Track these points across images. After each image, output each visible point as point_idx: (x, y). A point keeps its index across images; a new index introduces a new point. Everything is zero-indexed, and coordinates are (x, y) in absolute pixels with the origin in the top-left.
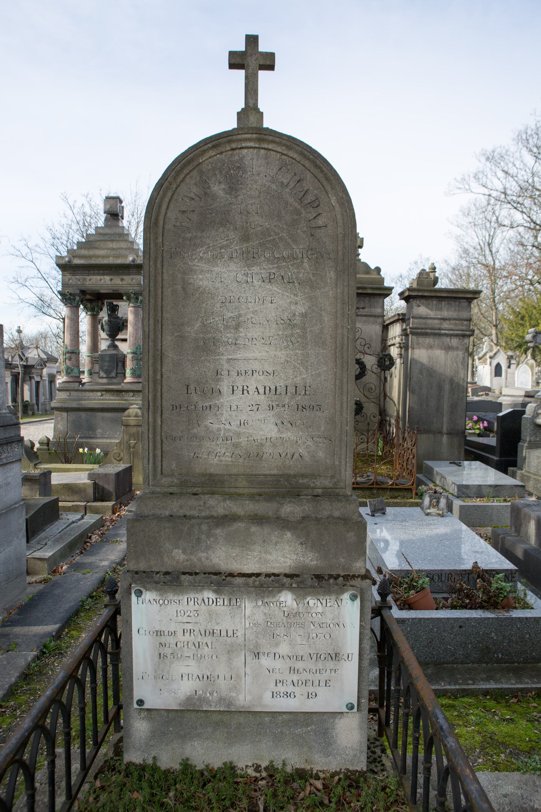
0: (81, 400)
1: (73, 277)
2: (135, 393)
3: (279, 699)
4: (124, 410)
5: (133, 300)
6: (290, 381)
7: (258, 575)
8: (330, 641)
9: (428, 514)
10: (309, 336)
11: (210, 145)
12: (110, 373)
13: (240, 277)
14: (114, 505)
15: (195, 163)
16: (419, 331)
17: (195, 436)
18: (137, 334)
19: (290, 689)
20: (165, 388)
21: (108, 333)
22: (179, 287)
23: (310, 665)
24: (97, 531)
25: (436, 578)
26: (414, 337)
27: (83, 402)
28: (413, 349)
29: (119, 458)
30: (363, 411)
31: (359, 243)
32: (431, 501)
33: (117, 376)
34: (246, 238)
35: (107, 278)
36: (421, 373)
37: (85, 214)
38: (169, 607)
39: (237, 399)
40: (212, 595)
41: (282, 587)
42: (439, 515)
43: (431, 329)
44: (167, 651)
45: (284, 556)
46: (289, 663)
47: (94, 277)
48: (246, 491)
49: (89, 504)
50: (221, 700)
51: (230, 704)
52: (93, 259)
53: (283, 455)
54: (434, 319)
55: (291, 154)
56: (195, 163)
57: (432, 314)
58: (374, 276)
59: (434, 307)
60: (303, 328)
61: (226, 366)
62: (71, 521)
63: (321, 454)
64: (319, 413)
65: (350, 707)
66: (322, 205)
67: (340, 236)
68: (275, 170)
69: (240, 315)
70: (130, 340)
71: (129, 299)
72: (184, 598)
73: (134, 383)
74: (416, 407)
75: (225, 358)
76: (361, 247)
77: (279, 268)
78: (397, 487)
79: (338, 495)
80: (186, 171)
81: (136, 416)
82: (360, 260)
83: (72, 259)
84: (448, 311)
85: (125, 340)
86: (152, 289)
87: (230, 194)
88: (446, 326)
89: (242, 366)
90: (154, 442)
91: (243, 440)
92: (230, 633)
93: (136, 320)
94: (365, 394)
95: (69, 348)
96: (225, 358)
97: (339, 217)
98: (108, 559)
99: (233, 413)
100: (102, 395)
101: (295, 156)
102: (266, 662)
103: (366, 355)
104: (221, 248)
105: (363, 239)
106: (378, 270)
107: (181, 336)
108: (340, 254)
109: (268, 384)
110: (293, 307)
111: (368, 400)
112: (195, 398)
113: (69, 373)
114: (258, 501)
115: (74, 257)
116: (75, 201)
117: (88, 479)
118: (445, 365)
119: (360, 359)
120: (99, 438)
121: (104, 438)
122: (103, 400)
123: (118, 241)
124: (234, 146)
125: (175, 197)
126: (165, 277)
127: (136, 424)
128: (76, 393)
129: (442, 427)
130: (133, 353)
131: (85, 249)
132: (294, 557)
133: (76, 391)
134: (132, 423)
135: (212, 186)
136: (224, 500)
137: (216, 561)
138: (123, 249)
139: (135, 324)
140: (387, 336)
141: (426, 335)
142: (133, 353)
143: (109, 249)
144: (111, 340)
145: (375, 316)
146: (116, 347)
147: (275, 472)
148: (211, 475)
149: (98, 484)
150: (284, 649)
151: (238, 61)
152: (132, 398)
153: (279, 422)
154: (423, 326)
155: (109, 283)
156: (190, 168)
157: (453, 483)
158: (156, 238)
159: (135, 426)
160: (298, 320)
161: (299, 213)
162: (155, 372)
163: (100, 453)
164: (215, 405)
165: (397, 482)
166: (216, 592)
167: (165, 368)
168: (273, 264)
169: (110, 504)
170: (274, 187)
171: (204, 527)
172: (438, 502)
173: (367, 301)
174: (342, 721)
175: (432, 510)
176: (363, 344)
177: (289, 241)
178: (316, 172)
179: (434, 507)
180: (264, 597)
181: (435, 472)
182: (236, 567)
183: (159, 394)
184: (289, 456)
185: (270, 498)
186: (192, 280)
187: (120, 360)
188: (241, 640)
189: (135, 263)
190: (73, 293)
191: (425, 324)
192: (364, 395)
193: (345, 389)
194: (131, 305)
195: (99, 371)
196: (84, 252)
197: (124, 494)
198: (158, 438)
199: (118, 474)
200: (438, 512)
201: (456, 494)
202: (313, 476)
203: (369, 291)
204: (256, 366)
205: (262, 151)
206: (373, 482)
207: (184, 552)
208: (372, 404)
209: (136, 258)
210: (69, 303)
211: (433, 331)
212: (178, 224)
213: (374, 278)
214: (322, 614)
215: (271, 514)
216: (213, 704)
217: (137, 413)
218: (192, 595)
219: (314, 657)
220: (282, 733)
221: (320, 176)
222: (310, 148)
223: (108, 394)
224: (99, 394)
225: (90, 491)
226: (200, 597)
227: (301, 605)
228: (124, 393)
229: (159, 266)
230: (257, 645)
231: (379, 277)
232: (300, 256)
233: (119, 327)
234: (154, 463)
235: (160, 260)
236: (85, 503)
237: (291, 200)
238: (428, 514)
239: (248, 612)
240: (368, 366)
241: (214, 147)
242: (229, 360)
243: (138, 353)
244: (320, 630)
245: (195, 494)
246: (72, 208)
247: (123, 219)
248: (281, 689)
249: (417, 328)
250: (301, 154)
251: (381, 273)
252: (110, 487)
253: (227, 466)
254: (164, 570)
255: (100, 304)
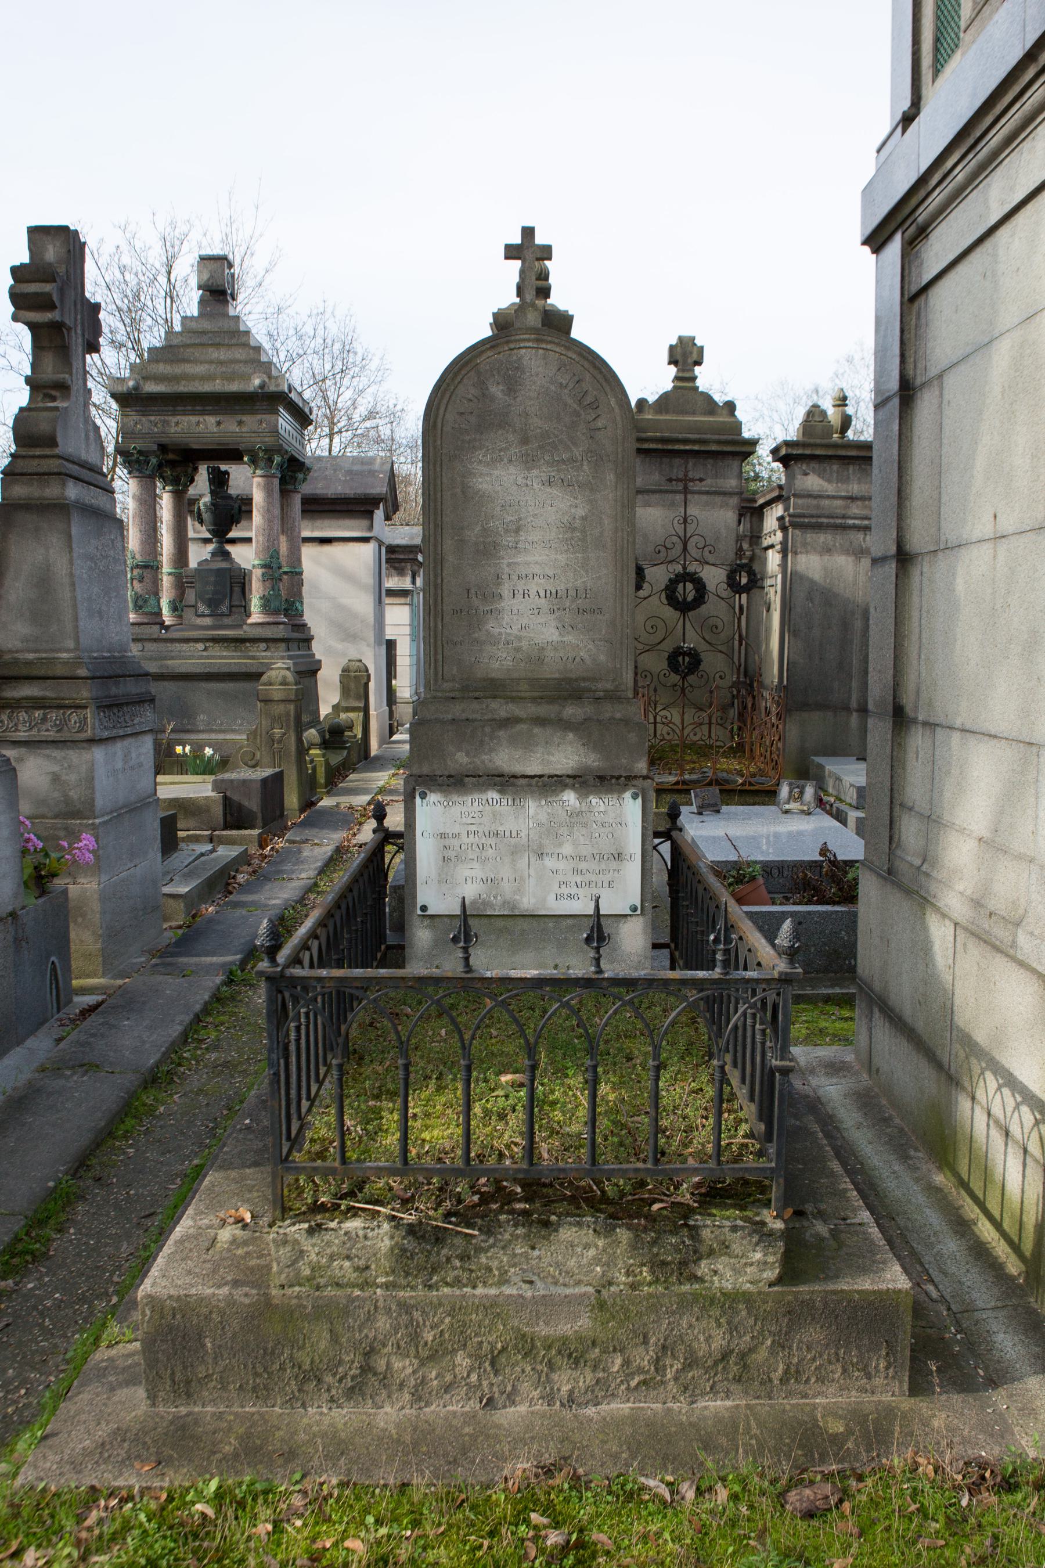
0: (165, 658)
1: (144, 419)
2: (270, 644)
3: (563, 902)
4: (256, 676)
5: (262, 464)
6: (570, 584)
7: (540, 776)
8: (612, 841)
9: (787, 812)
10: (589, 539)
11: (488, 346)
12: (217, 606)
13: (520, 481)
14: (260, 834)
15: (473, 364)
16: (806, 520)
17: (476, 640)
18: (271, 529)
19: (574, 890)
20: (445, 594)
21: (211, 528)
22: (458, 490)
23: (593, 865)
24: (245, 868)
25: (775, 872)
26: (797, 532)
27: (169, 662)
28: (796, 553)
29: (253, 762)
30: (701, 668)
31: (695, 357)
32: (791, 792)
33: (231, 611)
34: (525, 441)
35: (211, 420)
36: (810, 598)
37: (123, 270)
38: (453, 809)
39: (518, 603)
40: (496, 796)
41: (565, 786)
42: (803, 812)
43: (828, 517)
44: (452, 854)
45: (566, 757)
46: (572, 864)
47: (186, 418)
48: (528, 694)
49: (217, 833)
50: (505, 903)
51: (514, 907)
52: (183, 382)
53: (564, 659)
54: (834, 497)
55: (570, 354)
56: (473, 364)
57: (830, 488)
58: (723, 418)
59: (835, 475)
60: (584, 531)
61: (507, 570)
62: (198, 852)
63: (602, 658)
64: (599, 617)
65: (634, 909)
66: (601, 407)
67: (620, 438)
68: (554, 371)
69: (520, 519)
70: (258, 542)
71: (254, 462)
72: (468, 799)
73: (268, 623)
74: (801, 661)
75: (506, 561)
76: (699, 363)
77: (558, 471)
78: (752, 788)
79: (619, 698)
80: (463, 372)
81: (284, 683)
82: (698, 388)
83: (141, 382)
84: (859, 483)
85: (248, 540)
86: (432, 493)
87: (509, 395)
88: (856, 511)
89: (523, 570)
90: (435, 646)
91: (524, 644)
92: (514, 834)
93: (269, 503)
94: (707, 638)
95: (139, 557)
96: (506, 561)
97: (618, 418)
98: (278, 898)
99: (515, 617)
100: (205, 649)
101: (574, 356)
102: (549, 862)
103: (706, 567)
104: (501, 450)
105: (702, 348)
106: (731, 406)
107: (461, 541)
108: (620, 456)
109: (548, 588)
110: (573, 511)
111: (709, 648)
112: (476, 602)
113: (141, 607)
114: (540, 704)
115: (145, 378)
116: (102, 240)
117: (213, 791)
118: (855, 583)
119: (696, 573)
120: (203, 731)
121: (212, 731)
122: (208, 657)
123: (229, 346)
124: (512, 346)
125: (453, 398)
126: (445, 480)
127: (284, 698)
128: (155, 644)
129: (850, 698)
130: (264, 566)
131: (165, 362)
132: (577, 758)
133: (155, 640)
134: (277, 696)
135: (490, 387)
136: (507, 703)
137: (499, 763)
138: (240, 362)
139: (267, 511)
140: (761, 530)
141: (818, 527)
142: (264, 566)
143: (211, 362)
144: (218, 542)
145: (724, 494)
146: (226, 555)
147: (557, 676)
148: (492, 680)
149: (230, 799)
150: (567, 849)
151: (515, 253)
152: (264, 654)
153: (560, 625)
154: (814, 512)
155: (215, 430)
156: (468, 368)
157: (851, 785)
158: (435, 441)
159: (283, 701)
160: (578, 523)
161: (578, 415)
162: (436, 576)
163: (213, 755)
164: (496, 609)
165: (752, 780)
166: (500, 792)
167: (445, 572)
168: (552, 467)
169: (256, 832)
170: (553, 388)
171: (487, 729)
172: (802, 793)
173: (709, 466)
174: (626, 925)
175: (793, 806)
176: (701, 545)
177: (569, 443)
178: (596, 373)
179: (795, 800)
180: (547, 796)
181: (827, 773)
182: (518, 768)
183: (440, 599)
184: (570, 659)
185: (552, 700)
186: (471, 484)
187: (238, 581)
188: (524, 840)
189: (266, 390)
190: (144, 449)
191: (818, 507)
192: (704, 638)
193: (625, 592)
194: (259, 472)
195: (196, 602)
196: (162, 368)
197: (274, 820)
198: (439, 643)
199: (265, 781)
200: (801, 808)
201: (854, 803)
202: (594, 679)
203: (714, 448)
204: (537, 570)
205: (541, 351)
206: (711, 780)
207: (467, 755)
208: (720, 656)
209: (267, 380)
210: (137, 470)
211: (832, 521)
212: (457, 426)
213: (724, 422)
214: (604, 813)
215: (553, 716)
216: (497, 908)
217: (285, 677)
218: (476, 796)
219: (597, 857)
220: (566, 939)
221: (599, 377)
222: (589, 348)
223: (217, 647)
224: (200, 646)
225: (218, 811)
226: (484, 797)
227: (583, 804)
228: (248, 644)
229: (438, 469)
230: (541, 846)
231: (733, 419)
232: (580, 458)
233: (233, 516)
234: (436, 668)
235: (439, 463)
236: (209, 832)
237: (570, 401)
238: (787, 812)
239: (532, 811)
240: (711, 586)
241: (492, 347)
242: (509, 564)
243: (274, 566)
244: (603, 830)
245: (476, 698)
246: (96, 256)
247: (234, 299)
248: (565, 891)
249: (804, 516)
250: (580, 354)
251: (736, 413)
252: (253, 804)
253: (508, 670)
254: (447, 773)
255: (190, 470)
